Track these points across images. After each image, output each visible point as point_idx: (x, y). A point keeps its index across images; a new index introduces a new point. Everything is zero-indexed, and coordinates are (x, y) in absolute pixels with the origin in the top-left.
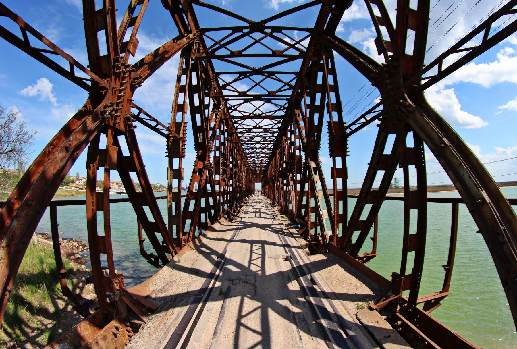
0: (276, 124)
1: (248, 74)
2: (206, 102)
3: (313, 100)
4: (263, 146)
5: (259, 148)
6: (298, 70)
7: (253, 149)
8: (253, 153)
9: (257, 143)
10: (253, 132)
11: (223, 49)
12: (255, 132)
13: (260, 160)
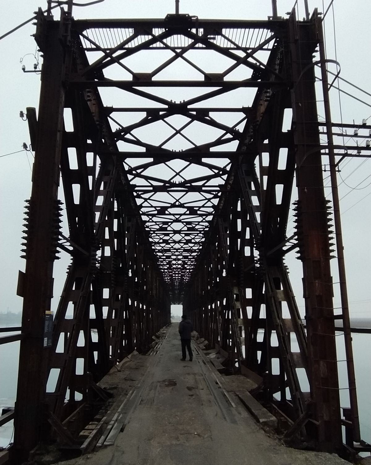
0: (209, 200)
1: (161, 113)
2: (90, 163)
3: (274, 159)
4: (188, 238)
5: (179, 242)
6: (249, 104)
7: (169, 244)
8: (169, 250)
9: (175, 232)
10: (170, 214)
11: (116, 64)
12: (174, 215)
13: (180, 262)
